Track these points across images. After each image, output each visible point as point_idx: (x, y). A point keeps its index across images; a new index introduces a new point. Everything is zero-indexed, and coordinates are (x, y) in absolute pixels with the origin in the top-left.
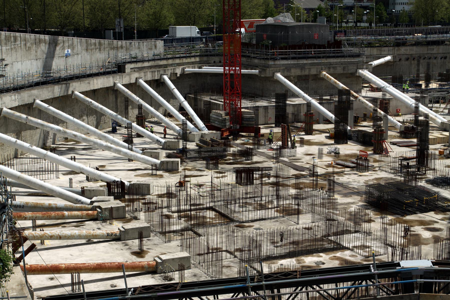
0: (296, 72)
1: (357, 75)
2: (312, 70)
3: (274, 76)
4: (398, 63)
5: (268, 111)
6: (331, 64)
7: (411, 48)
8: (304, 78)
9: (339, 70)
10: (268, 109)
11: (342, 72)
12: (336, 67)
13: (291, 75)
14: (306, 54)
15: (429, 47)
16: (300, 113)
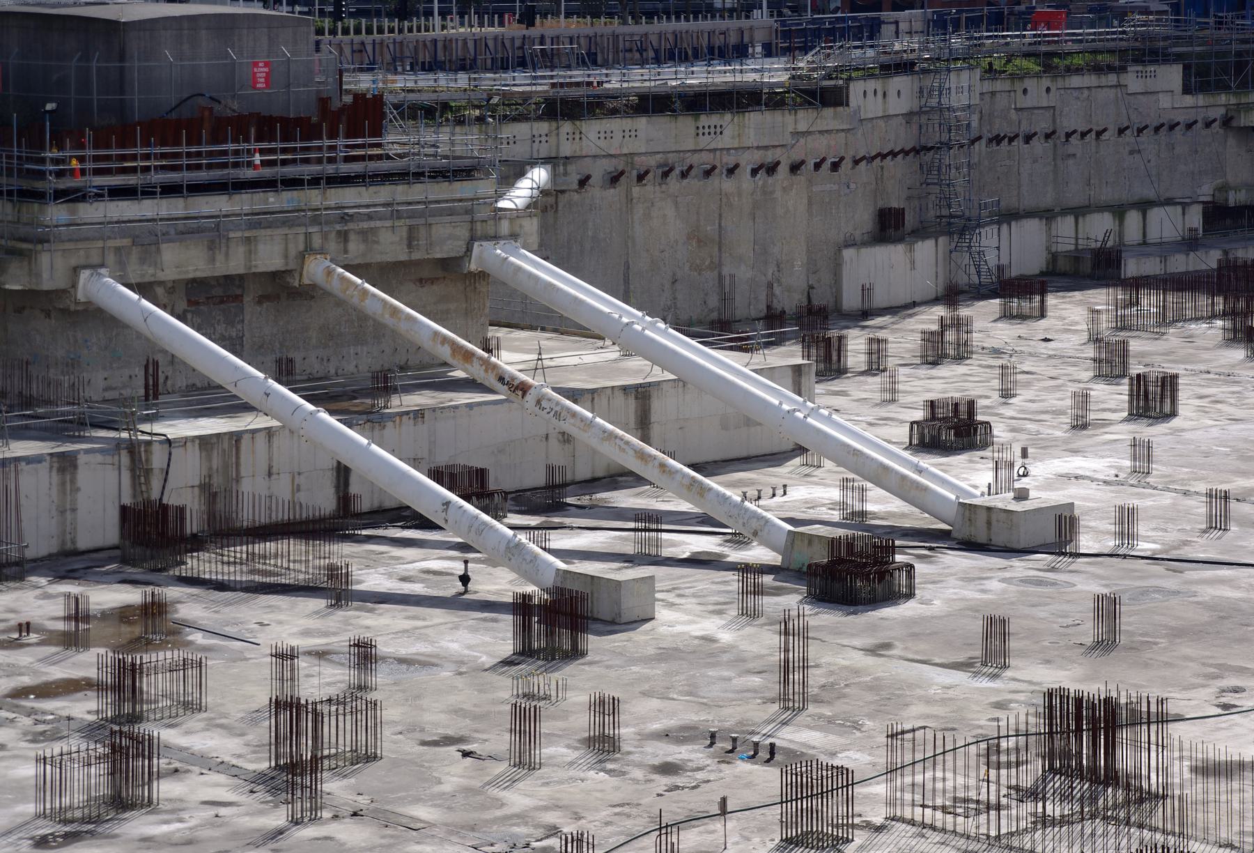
0: (183, 261)
1: (473, 267)
2: (261, 247)
3: (74, 286)
4: (576, 197)
5: (73, 481)
6: (344, 219)
7: (627, 123)
8: (218, 292)
9: (390, 245)
10: (75, 466)
11: (403, 257)
12: (373, 231)
13: (161, 276)
14: (224, 166)
15: (704, 120)
16: (238, 479)
